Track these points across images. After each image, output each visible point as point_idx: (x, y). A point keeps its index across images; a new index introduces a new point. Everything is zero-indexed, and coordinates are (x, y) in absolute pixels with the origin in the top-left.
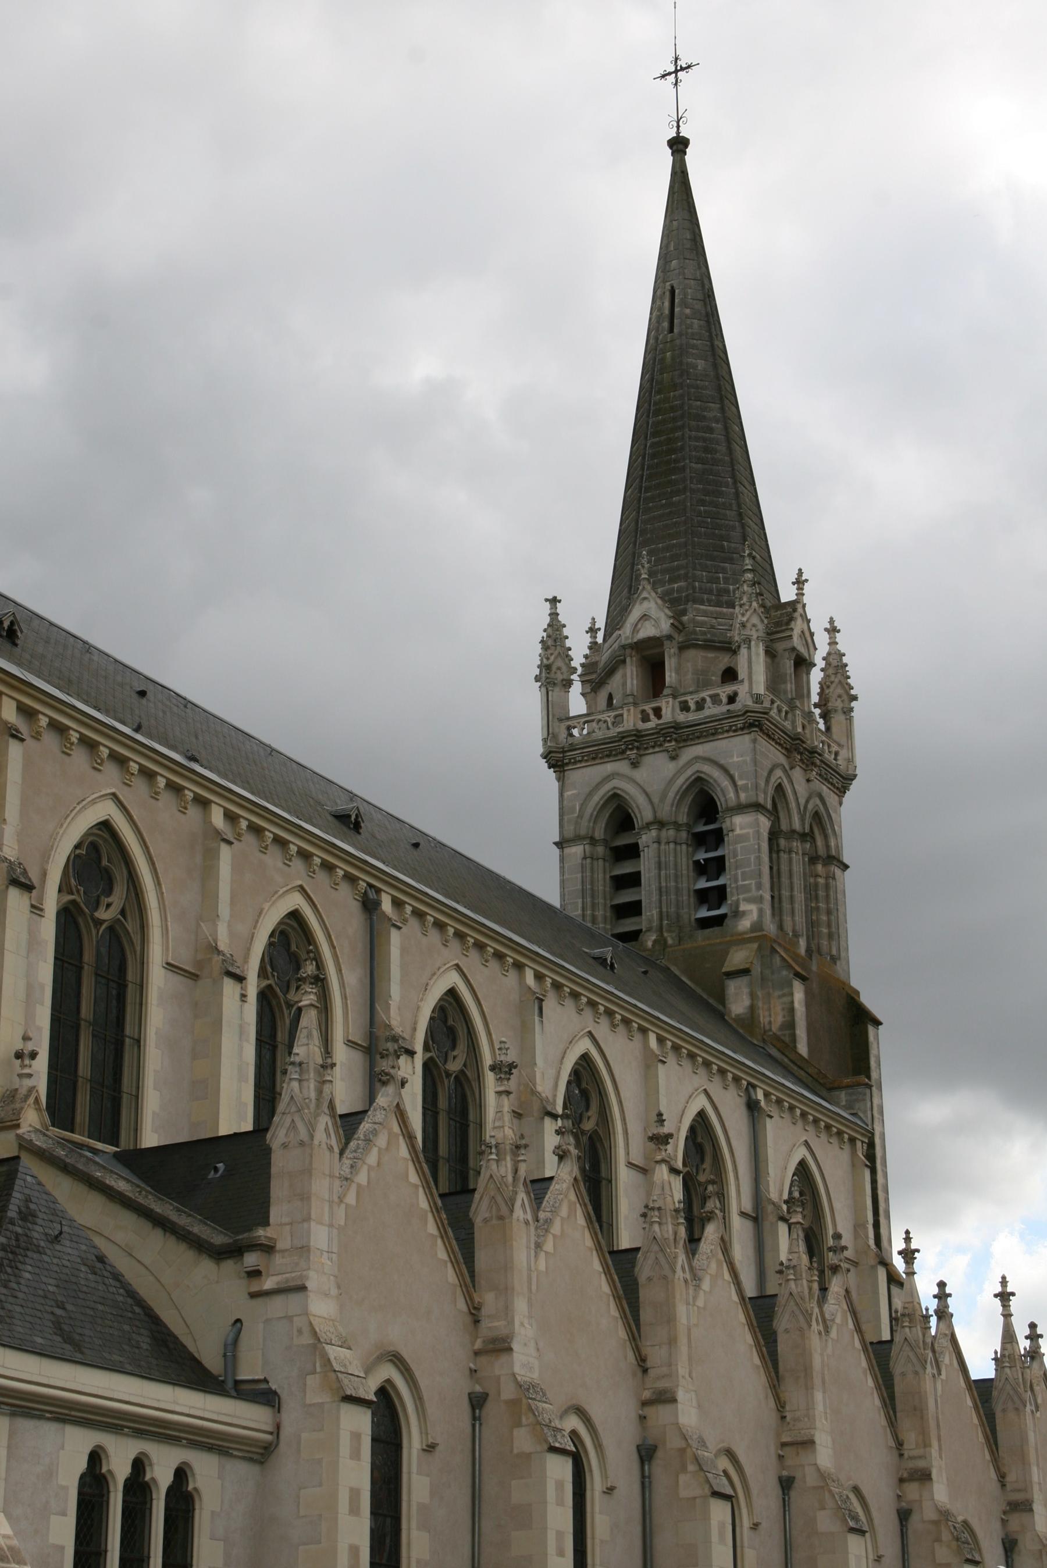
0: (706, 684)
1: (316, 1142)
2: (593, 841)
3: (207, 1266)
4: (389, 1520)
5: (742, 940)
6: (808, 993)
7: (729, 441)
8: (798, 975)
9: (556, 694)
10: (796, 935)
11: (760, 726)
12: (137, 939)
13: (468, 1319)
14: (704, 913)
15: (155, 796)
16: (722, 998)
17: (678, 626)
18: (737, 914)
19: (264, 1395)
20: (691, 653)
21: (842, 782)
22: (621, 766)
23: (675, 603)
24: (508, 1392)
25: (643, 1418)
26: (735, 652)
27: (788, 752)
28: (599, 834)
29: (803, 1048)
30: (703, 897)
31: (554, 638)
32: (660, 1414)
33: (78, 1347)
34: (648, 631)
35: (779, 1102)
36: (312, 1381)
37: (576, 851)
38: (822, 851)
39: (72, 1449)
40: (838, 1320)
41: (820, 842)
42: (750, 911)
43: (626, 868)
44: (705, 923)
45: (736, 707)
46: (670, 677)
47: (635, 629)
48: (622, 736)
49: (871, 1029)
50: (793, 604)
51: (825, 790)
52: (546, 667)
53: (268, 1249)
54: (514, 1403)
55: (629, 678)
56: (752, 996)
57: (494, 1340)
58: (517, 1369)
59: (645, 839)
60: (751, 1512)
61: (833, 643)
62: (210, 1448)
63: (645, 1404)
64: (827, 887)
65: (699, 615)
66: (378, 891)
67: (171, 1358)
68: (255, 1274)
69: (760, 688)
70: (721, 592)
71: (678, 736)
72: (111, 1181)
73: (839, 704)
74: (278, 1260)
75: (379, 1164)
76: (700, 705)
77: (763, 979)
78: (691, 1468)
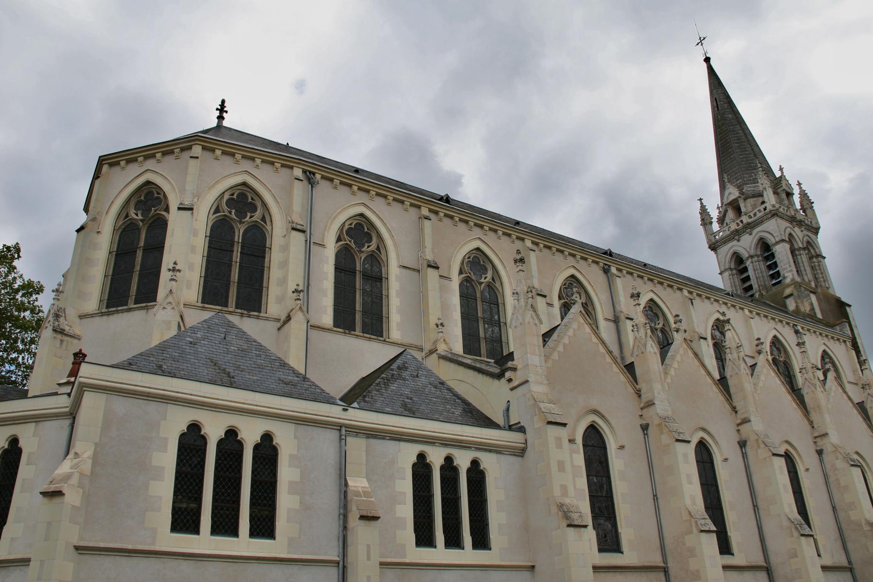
0: (756, 207)
1: (526, 321)
2: (731, 269)
3: (496, 382)
4: (604, 478)
5: (789, 286)
6: (818, 299)
7: (745, 135)
8: (811, 292)
9: (708, 227)
10: (810, 281)
11: (777, 214)
12: (500, 289)
13: (635, 395)
14: (774, 282)
15: (499, 238)
16: (785, 306)
17: (742, 193)
18: (785, 278)
19: (522, 430)
20: (749, 200)
21: (816, 230)
22: (735, 243)
23: (740, 188)
24: (656, 421)
25: (738, 431)
26: (762, 196)
27: (791, 222)
28: (733, 266)
29: (819, 316)
30: (772, 277)
31: (704, 211)
32: (744, 428)
33: (414, 413)
34: (732, 198)
35: (809, 330)
36: (536, 418)
37: (726, 274)
38: (814, 254)
39: (408, 454)
40: (834, 389)
41: (812, 251)
42: (789, 273)
43: (745, 275)
44: (774, 285)
45: (768, 210)
46: (743, 209)
47: (728, 198)
48: (732, 233)
49: (847, 308)
50: (781, 177)
51: (810, 234)
52: (703, 220)
53: (514, 369)
54: (659, 425)
55: (731, 214)
56: (796, 302)
57: (648, 402)
58: (659, 411)
59: (748, 263)
60: (803, 464)
61: (801, 188)
62: (486, 450)
63: (738, 425)
64: (819, 265)
65: (748, 188)
66: (609, 266)
67: (475, 416)
68: (510, 380)
69: (774, 202)
70: (754, 179)
71: (749, 227)
72: (465, 361)
73: (808, 206)
74: (518, 373)
75: (574, 335)
76: (755, 215)
77: (799, 296)
78: (762, 446)
